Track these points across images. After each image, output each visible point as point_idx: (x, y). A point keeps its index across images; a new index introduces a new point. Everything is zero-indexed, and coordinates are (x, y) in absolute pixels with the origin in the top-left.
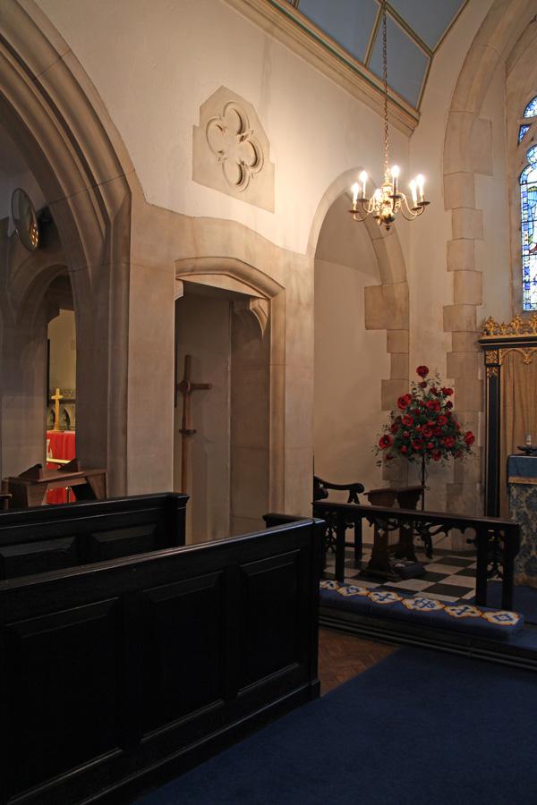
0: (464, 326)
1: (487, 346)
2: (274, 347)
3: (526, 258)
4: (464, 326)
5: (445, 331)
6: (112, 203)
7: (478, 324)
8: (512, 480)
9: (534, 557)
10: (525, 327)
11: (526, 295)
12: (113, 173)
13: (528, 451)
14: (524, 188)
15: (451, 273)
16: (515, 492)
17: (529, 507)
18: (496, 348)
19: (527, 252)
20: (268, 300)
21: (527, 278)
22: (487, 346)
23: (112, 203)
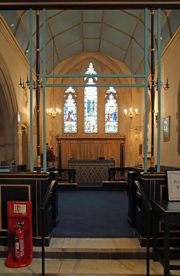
0: (54, 135)
1: (58, 140)
2: (65, 260)
3: (65, 122)
4: (54, 135)
5: (50, 136)
6: (15, 111)
7: (57, 134)
8: (69, 164)
9: (20, 223)
10: (66, 136)
11: (65, 129)
12: (16, 106)
13: (71, 159)
14: (65, 107)
15: (51, 124)
16: (70, 166)
17: (87, 169)
18: (60, 140)
19: (65, 121)
20: (27, 129)
21: (65, 126)
22: (58, 140)
23: (15, 111)
